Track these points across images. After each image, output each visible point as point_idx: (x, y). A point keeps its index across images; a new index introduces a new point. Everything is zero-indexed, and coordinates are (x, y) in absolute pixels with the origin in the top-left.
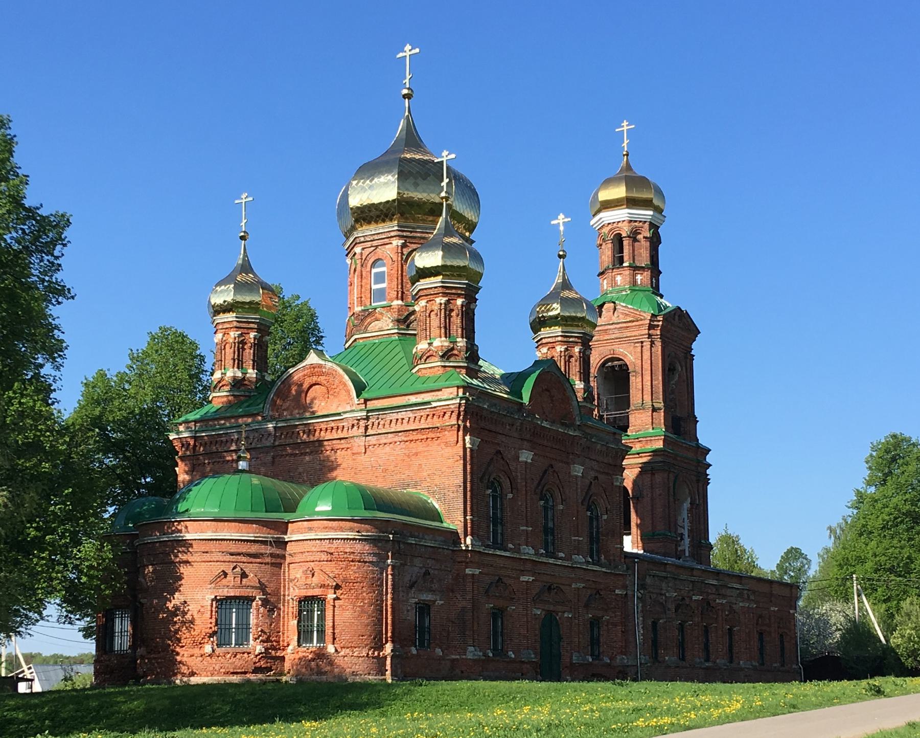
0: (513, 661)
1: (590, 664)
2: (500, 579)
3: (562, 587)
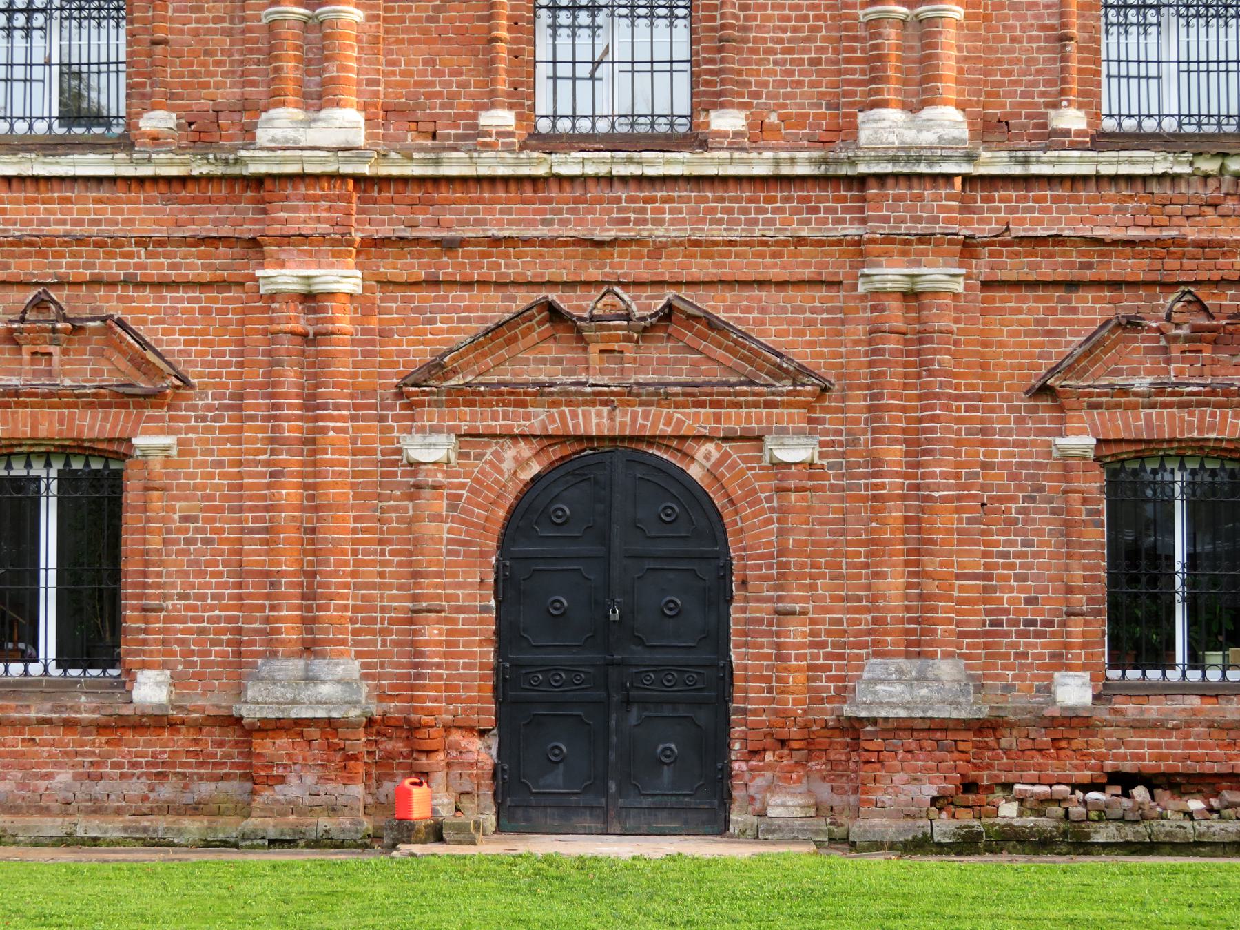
0: (157, 722)
1: (1074, 723)
2: (40, 304)
3: (712, 303)
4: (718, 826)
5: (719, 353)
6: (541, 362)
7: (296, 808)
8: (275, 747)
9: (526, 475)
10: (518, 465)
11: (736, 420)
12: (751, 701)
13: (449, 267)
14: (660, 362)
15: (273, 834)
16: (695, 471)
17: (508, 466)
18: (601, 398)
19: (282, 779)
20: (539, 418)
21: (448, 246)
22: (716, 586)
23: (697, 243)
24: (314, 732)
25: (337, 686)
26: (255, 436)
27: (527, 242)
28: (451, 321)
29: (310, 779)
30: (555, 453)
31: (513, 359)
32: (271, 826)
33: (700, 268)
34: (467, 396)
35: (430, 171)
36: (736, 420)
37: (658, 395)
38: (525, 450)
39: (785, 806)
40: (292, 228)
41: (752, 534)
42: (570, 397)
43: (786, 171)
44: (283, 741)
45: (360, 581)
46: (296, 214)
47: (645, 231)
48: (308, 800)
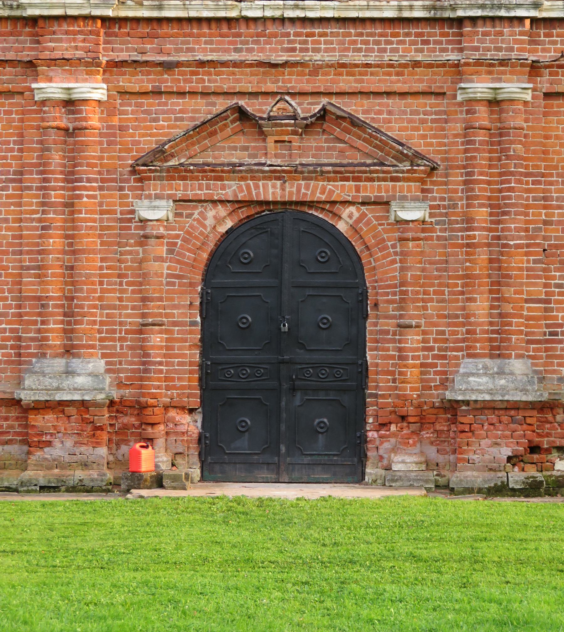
3: (354, 107)
4: (356, 476)
5: (359, 143)
6: (233, 149)
7: (59, 464)
8: (44, 421)
9: (222, 229)
10: (217, 222)
11: (371, 190)
12: (381, 389)
13: (168, 82)
14: (318, 150)
15: (42, 482)
16: (341, 226)
17: (210, 222)
18: (276, 175)
19: (49, 444)
20: (232, 189)
21: (168, 67)
22: (355, 306)
23: (343, 65)
24: (71, 410)
25: (88, 378)
26: (31, 201)
27: (224, 64)
28: (170, 120)
29: (69, 443)
30: (243, 213)
31: (213, 147)
32: (42, 477)
33: (346, 83)
34: (181, 173)
35: (155, 14)
36: (371, 190)
37: (316, 173)
38: (222, 211)
39: (405, 462)
40: (58, 54)
41: (382, 271)
42: (253, 173)
43: (406, 14)
44: (50, 417)
45: (105, 304)
46: (60, 44)
47: (307, 57)
48: (67, 459)
